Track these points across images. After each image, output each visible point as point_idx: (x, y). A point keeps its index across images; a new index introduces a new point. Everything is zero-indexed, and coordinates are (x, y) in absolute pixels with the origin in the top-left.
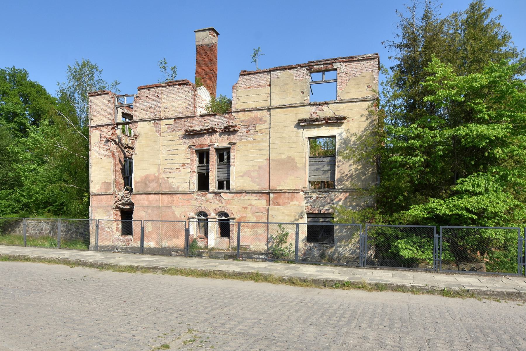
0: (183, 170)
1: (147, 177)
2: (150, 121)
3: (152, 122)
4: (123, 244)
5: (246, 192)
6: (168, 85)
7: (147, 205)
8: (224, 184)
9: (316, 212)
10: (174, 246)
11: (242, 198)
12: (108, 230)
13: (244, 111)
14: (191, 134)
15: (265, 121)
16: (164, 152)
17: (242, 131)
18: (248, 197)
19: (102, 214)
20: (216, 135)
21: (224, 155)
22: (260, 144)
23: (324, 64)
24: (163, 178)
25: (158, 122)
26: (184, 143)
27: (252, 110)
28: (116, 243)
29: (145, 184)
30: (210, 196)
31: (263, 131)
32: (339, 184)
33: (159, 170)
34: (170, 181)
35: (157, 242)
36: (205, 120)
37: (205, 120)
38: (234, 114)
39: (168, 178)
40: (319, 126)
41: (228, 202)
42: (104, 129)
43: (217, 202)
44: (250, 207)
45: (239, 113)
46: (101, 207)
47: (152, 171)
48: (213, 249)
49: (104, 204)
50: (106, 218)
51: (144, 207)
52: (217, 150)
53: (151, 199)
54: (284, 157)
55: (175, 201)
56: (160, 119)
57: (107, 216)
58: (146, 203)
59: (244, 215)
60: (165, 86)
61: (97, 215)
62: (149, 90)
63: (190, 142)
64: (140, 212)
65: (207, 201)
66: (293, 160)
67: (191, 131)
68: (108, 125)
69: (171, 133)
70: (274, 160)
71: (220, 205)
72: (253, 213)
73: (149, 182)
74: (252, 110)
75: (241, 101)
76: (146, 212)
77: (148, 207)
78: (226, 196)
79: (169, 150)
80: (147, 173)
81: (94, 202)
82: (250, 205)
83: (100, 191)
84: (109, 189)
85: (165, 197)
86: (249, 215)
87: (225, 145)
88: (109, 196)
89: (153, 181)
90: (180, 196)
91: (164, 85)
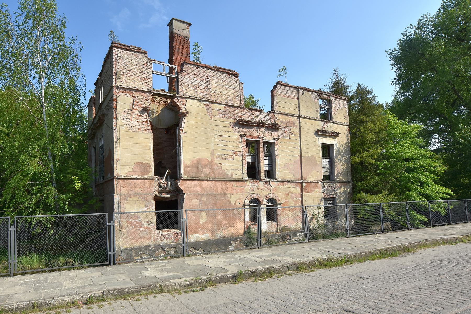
0: (235, 157)
1: (199, 161)
2: (201, 101)
3: (203, 102)
4: (169, 241)
5: (288, 181)
6: (217, 70)
7: (199, 193)
8: (271, 174)
9: (328, 197)
10: (230, 235)
11: (284, 186)
12: (147, 225)
13: (283, 114)
14: (241, 123)
15: (297, 126)
16: (216, 137)
17: (282, 130)
18: (289, 185)
19: (133, 205)
20: (263, 129)
21: (270, 146)
22: (294, 143)
23: (326, 95)
24: (216, 163)
25: (209, 104)
26: (235, 132)
27: (288, 115)
28: (159, 241)
29: (198, 169)
30: (261, 184)
31: (295, 133)
32: (337, 178)
33: (212, 154)
34: (224, 167)
35: (213, 233)
36: (253, 114)
37: (253, 114)
38: (276, 115)
39: (221, 164)
40: (326, 136)
41: (275, 189)
42: (140, 97)
43: (267, 189)
44: (290, 194)
45: (279, 115)
46: (134, 196)
47: (206, 155)
48: (266, 233)
49: (139, 191)
50: (145, 209)
51: (198, 196)
52: (265, 143)
53: (204, 186)
54: (310, 155)
55: (229, 188)
56: (212, 102)
57: (146, 207)
58: (199, 190)
59: (287, 200)
60: (214, 70)
61: (127, 206)
62: (197, 68)
63: (241, 131)
64: (193, 201)
65: (258, 188)
66: (315, 158)
67: (245, 122)
68: (145, 92)
69: (222, 119)
70: (304, 157)
71: (269, 192)
72: (293, 198)
73: (202, 167)
74: (288, 115)
75: (280, 105)
76: (200, 201)
77: (202, 195)
78: (273, 184)
79: (221, 136)
80: (198, 157)
81: (119, 191)
82: (290, 192)
83: (132, 173)
84: (147, 172)
85: (219, 184)
86: (290, 200)
87: (270, 140)
88: (147, 182)
89: (206, 166)
90: (234, 184)
91: (213, 68)
